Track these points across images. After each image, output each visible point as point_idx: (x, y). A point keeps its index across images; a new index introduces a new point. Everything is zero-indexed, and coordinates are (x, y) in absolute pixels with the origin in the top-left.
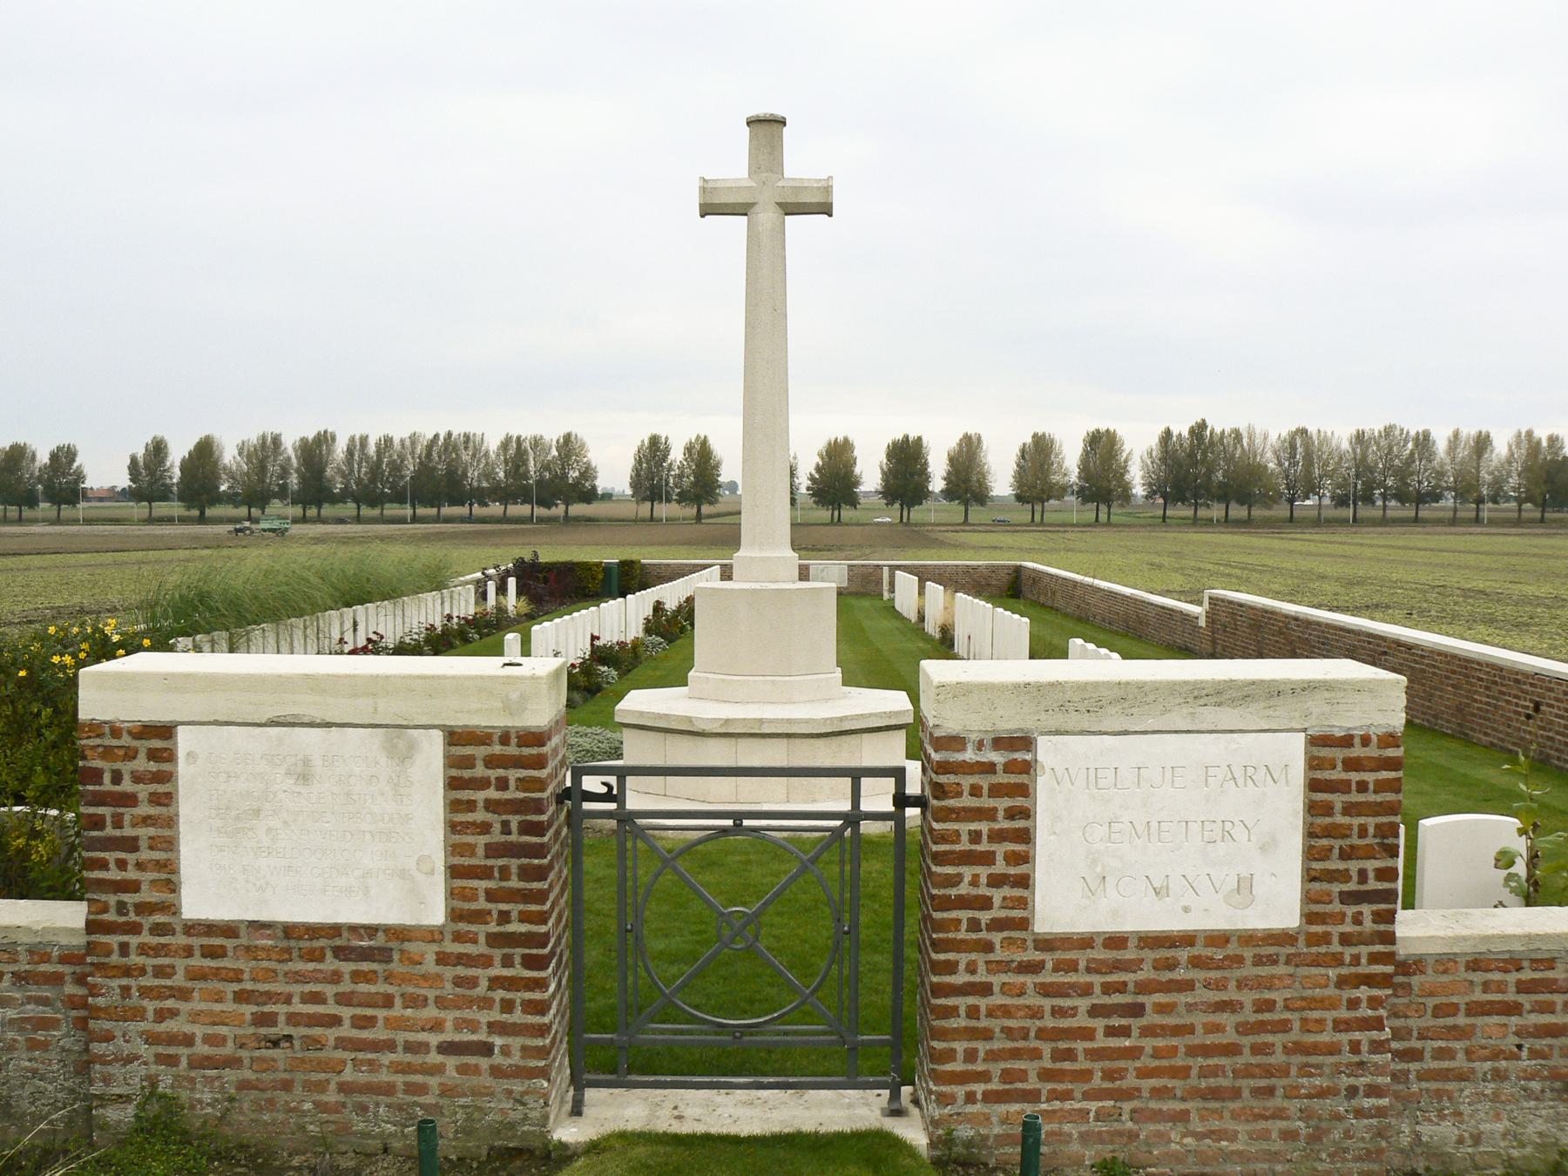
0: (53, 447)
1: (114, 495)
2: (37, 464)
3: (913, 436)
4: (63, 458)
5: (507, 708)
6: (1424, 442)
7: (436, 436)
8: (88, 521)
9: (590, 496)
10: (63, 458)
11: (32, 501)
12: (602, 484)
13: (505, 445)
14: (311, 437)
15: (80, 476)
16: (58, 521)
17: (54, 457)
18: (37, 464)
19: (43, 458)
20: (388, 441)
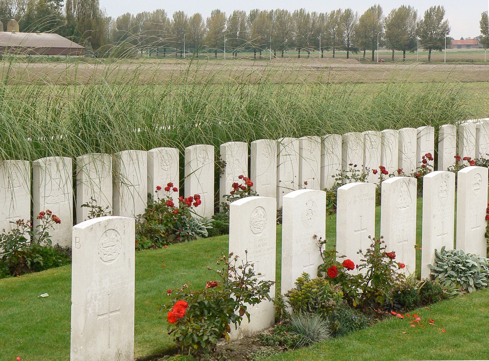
0: (428, 8)
1: (465, 44)
2: (418, 20)
3: (181, 11)
4: (435, 15)
5: (384, 191)
6: (197, 18)
7: (272, 11)
8: (449, 61)
9: (449, 43)
10: (435, 15)
11: (411, 46)
12: (455, 34)
13: (320, 14)
14: (291, 12)
15: (446, 30)
16: (429, 61)
17: (428, 15)
18: (418, 20)
19: (421, 17)
20: (217, 15)
